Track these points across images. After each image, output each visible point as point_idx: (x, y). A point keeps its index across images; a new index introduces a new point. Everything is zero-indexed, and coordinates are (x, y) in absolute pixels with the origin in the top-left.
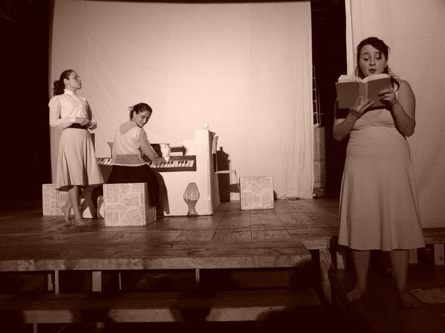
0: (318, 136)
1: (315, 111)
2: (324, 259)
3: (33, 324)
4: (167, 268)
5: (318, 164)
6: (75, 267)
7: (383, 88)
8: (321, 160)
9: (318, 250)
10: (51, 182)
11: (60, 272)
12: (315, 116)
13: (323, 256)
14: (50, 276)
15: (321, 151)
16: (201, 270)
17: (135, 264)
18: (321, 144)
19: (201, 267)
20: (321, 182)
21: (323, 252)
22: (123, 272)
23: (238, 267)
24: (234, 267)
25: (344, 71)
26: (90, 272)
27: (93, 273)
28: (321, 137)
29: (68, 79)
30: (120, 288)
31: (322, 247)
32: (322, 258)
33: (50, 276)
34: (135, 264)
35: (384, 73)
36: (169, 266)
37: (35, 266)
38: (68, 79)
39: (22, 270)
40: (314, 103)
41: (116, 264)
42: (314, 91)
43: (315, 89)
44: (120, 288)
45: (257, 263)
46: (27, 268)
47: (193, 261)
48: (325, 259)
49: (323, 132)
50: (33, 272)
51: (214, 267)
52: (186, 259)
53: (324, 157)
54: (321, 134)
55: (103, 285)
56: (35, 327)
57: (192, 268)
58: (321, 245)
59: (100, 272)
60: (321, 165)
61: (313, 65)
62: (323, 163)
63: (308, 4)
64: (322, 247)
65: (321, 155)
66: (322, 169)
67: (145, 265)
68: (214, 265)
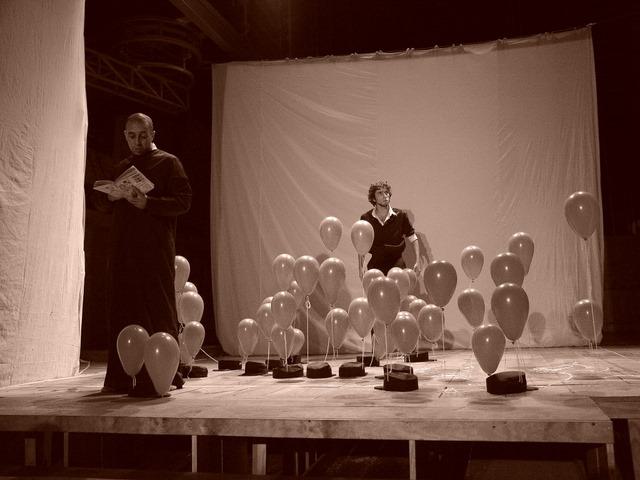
3: (190, 437)
4: (361, 438)
6: (220, 431)
7: (467, 246)
10: (82, 365)
11: (199, 437)
16: (417, 442)
17: (311, 430)
19: (418, 438)
21: (635, 425)
29: (494, 50)
34: (311, 430)
36: (364, 434)
37: (163, 427)
38: (494, 50)
39: (145, 433)
45: (514, 433)
46: (153, 430)
47: (288, 430)
51: (439, 438)
57: (189, 434)
67: (326, 432)
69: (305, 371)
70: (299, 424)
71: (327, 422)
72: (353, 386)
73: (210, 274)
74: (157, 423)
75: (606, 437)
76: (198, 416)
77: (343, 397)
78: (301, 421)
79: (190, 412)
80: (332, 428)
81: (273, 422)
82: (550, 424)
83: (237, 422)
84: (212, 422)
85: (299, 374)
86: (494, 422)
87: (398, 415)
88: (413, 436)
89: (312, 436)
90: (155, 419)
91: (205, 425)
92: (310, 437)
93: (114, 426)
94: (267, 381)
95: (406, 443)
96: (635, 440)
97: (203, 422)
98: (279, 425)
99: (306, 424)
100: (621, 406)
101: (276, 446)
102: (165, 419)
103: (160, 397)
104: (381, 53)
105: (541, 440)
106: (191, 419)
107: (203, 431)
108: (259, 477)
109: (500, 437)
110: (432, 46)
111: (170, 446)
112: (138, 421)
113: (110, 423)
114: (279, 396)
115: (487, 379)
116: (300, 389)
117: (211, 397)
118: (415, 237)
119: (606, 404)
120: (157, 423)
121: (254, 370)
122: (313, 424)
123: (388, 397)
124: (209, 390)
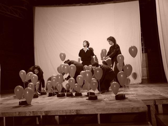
0: (144, 57)
1: (142, 46)
2: (152, 109)
3: (40, 116)
4: (90, 113)
5: (145, 69)
8: (146, 67)
9: (149, 105)
11: (42, 116)
12: (142, 49)
13: (152, 108)
14: (37, 118)
15: (146, 63)
16: (101, 114)
18: (146, 60)
19: (100, 113)
20: (147, 76)
21: (152, 106)
22: (14, 117)
23: (116, 112)
24: (114, 113)
25: (109, 59)
26: (54, 116)
27: (56, 116)
28: (146, 57)
30: (99, 123)
31: (151, 104)
32: (151, 108)
33: (37, 118)
34: (73, 112)
35: (76, 83)
40: (142, 43)
41: (65, 112)
42: (141, 38)
43: (142, 37)
44: (99, 123)
46: (30, 115)
47: (67, 113)
48: (153, 109)
49: (147, 55)
50: (150, 109)
51: (106, 113)
52: (94, 110)
53: (147, 66)
54: (146, 56)
55: (36, 118)
56: (4, 118)
57: (40, 115)
58: (151, 103)
59: (58, 116)
60: (147, 69)
61: (141, 27)
62: (147, 68)
63: (138, 2)
64: (151, 104)
65: (146, 64)
66: (147, 71)
68: (106, 112)
69: (66, 95)
70: (69, 111)
71: (77, 110)
72: (79, 99)
73: (166, 77)
74: (31, 113)
75: (146, 109)
76: (42, 110)
77: (78, 102)
78: (70, 110)
79: (39, 109)
80: (78, 112)
81: (63, 111)
82: (133, 108)
83: (53, 111)
84: (46, 112)
85: (64, 96)
86: (119, 108)
87: (95, 107)
88: (99, 113)
89: (73, 114)
90: (30, 112)
91: (44, 113)
92: (73, 114)
93: (19, 114)
94: (55, 98)
95: (98, 114)
96: (152, 110)
97: (44, 112)
98: (64, 111)
99: (72, 111)
100: (149, 102)
101: (60, 116)
102: (33, 112)
103: (28, 105)
104: (82, 4)
105: (131, 112)
106: (40, 111)
107: (44, 114)
108: (38, 124)
109: (121, 112)
110: (88, 3)
111: (33, 119)
112: (25, 113)
113: (18, 113)
114: (61, 103)
115: (115, 96)
116: (66, 100)
117: (42, 104)
118: (94, 57)
119: (145, 102)
120: (31, 113)
121: (51, 95)
122: (73, 111)
123: (90, 102)
124: (41, 102)
